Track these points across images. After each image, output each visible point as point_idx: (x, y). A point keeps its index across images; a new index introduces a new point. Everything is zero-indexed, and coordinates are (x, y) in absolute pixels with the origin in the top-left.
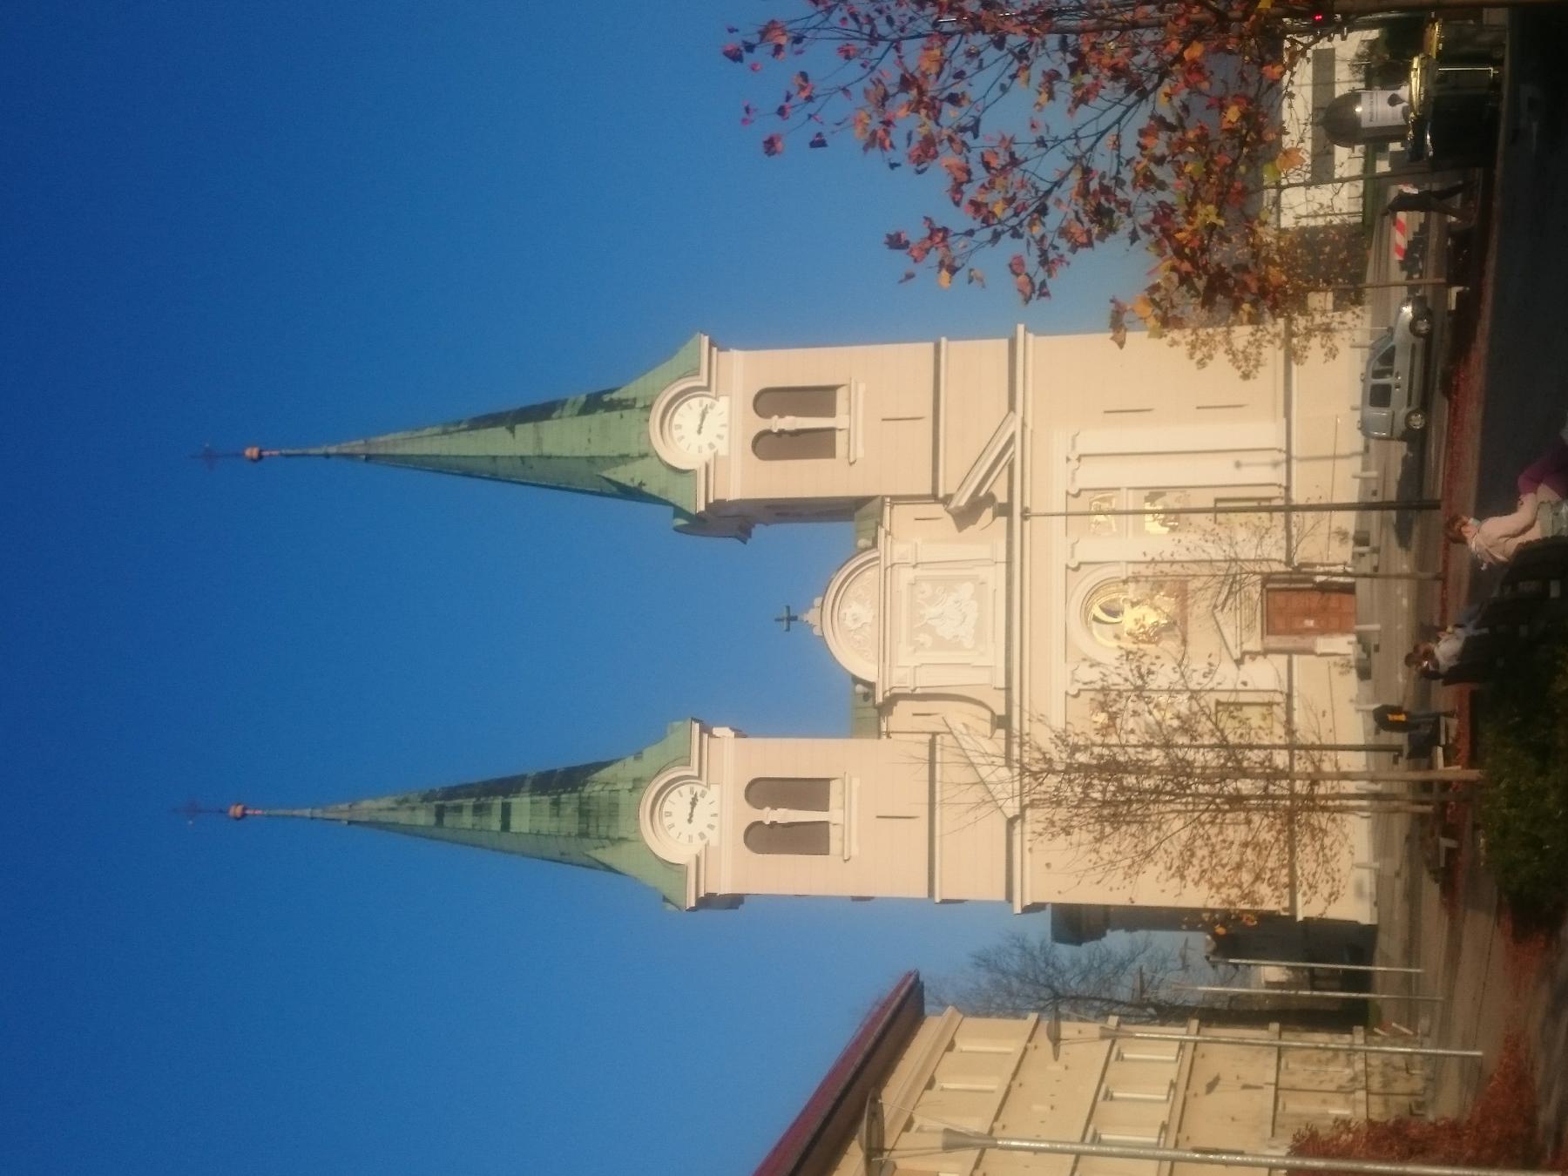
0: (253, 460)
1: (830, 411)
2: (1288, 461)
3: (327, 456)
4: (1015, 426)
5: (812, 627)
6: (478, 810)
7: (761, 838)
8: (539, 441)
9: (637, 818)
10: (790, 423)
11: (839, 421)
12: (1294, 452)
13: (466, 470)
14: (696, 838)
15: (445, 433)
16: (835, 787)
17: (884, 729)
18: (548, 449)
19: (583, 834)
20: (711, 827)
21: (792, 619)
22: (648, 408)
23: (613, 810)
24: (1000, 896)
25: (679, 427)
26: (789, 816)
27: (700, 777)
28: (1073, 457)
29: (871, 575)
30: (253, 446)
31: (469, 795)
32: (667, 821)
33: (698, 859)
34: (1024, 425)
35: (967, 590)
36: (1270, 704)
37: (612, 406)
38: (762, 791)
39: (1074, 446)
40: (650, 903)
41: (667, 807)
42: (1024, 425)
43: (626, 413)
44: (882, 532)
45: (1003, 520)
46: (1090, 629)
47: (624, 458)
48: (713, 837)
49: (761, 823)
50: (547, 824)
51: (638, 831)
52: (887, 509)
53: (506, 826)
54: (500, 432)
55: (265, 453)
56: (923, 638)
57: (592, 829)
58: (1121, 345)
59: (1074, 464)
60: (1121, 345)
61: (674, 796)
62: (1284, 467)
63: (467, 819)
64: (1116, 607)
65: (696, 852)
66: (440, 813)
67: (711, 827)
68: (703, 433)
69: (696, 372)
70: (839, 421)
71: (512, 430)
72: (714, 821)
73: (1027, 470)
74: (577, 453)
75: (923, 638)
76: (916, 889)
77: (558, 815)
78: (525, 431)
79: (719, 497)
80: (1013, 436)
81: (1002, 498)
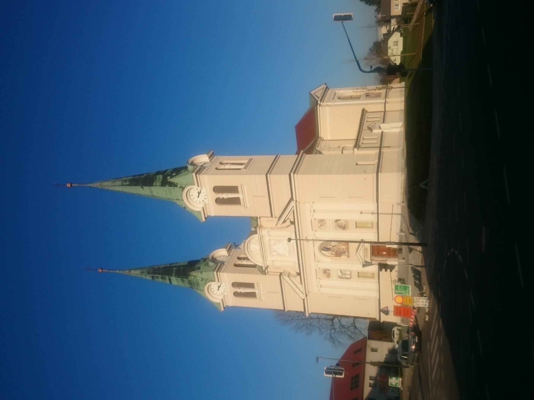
4: (293, 204)
6: (162, 278)
8: (152, 192)
12: (379, 212)
14: (202, 202)
15: (123, 185)
20: (205, 199)
22: (183, 189)
24: (303, 310)
25: (192, 195)
26: (244, 289)
33: (203, 208)
42: (296, 201)
48: (206, 201)
51: (182, 196)
52: (259, 220)
53: (171, 283)
56: (274, 253)
58: (320, 153)
59: (312, 212)
60: (320, 153)
62: (376, 215)
63: (160, 280)
64: (328, 247)
66: (153, 277)
67: (205, 199)
68: (199, 197)
72: (206, 197)
73: (297, 188)
75: (274, 253)
78: (146, 188)
79: (208, 215)
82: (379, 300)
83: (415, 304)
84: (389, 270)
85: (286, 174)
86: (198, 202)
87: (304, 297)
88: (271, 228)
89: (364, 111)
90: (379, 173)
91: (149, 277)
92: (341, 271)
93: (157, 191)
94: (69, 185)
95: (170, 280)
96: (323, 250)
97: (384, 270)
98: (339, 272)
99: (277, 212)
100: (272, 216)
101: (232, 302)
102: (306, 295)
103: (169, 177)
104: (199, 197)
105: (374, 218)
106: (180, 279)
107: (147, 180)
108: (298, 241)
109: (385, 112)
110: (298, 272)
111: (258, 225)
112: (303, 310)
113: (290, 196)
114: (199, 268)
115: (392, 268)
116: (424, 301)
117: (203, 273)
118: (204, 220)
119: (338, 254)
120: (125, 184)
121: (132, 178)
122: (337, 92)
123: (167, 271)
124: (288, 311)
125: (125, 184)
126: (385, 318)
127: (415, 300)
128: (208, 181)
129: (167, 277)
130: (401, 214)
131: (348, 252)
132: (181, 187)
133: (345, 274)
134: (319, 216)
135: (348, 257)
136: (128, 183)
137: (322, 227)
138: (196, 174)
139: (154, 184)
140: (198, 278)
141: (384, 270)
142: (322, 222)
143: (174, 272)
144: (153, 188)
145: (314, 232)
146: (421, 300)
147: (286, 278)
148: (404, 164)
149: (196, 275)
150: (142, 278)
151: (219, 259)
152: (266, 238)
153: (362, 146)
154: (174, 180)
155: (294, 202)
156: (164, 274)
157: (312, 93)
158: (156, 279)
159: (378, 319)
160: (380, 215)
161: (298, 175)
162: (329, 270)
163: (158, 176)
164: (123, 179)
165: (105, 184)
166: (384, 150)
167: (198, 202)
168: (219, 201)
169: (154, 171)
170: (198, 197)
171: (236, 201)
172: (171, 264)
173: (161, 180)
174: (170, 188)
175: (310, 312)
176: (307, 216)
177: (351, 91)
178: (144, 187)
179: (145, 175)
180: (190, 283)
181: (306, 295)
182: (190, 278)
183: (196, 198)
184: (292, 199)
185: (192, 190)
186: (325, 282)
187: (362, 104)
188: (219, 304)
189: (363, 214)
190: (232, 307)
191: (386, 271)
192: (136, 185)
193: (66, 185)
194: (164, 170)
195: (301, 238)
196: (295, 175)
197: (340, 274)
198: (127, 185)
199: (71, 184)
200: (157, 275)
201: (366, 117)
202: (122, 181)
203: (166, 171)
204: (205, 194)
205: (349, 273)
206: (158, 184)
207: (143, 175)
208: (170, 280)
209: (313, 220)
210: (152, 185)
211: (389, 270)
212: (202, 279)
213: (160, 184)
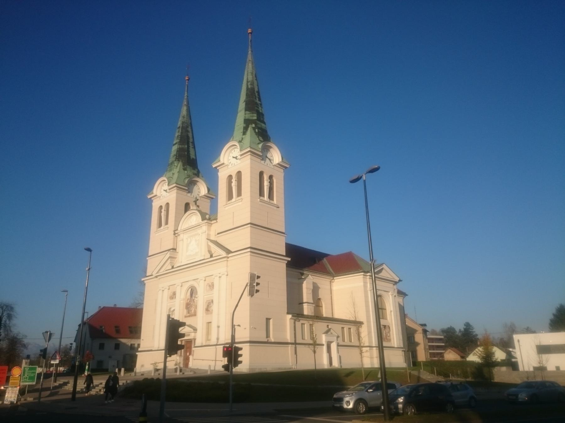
6: (178, 136)
8: (241, 111)
15: (248, 82)
24: (147, 275)
42: (228, 258)
63: (177, 134)
66: (179, 127)
75: (189, 240)
82: (151, 350)
83: (10, 389)
85: (251, 243)
87: (155, 275)
88: (209, 235)
89: (358, 324)
90: (248, 344)
91: (180, 124)
92: (174, 310)
93: (241, 115)
94: (250, 31)
95: (176, 144)
99: (221, 240)
101: (156, 205)
102: (156, 277)
103: (254, 125)
104: (233, 159)
109: (250, 342)
111: (211, 221)
112: (147, 275)
113: (233, 250)
114: (185, 169)
116: (12, 400)
118: (214, 166)
120: (249, 84)
121: (256, 89)
122: (390, 293)
123: (186, 140)
124: (147, 260)
125: (249, 84)
127: (15, 389)
130: (215, 370)
132: (242, 138)
136: (249, 87)
137: (208, 287)
139: (247, 112)
143: (183, 146)
144: (243, 111)
145: (204, 279)
146: (13, 396)
147: (168, 255)
148: (285, 369)
149: (178, 166)
150: (179, 117)
151: (195, 188)
152: (200, 231)
153: (298, 324)
155: (225, 255)
157: (384, 266)
158: (177, 130)
159: (139, 349)
160: (214, 347)
161: (249, 256)
163: (255, 115)
164: (255, 82)
165: (250, 65)
166: (290, 348)
169: (263, 110)
170: (233, 157)
172: (193, 143)
173: (251, 118)
176: (219, 268)
177: (392, 309)
179: (259, 102)
180: (172, 163)
181: (156, 277)
183: (232, 155)
184: (228, 252)
186: (167, 294)
187: (369, 321)
188: (153, 193)
194: (265, 121)
196: (249, 254)
197: (172, 310)
199: (251, 33)
201: (350, 326)
202: (253, 81)
203: (265, 123)
207: (260, 100)
208: (176, 144)
209: (213, 277)
213: (247, 118)
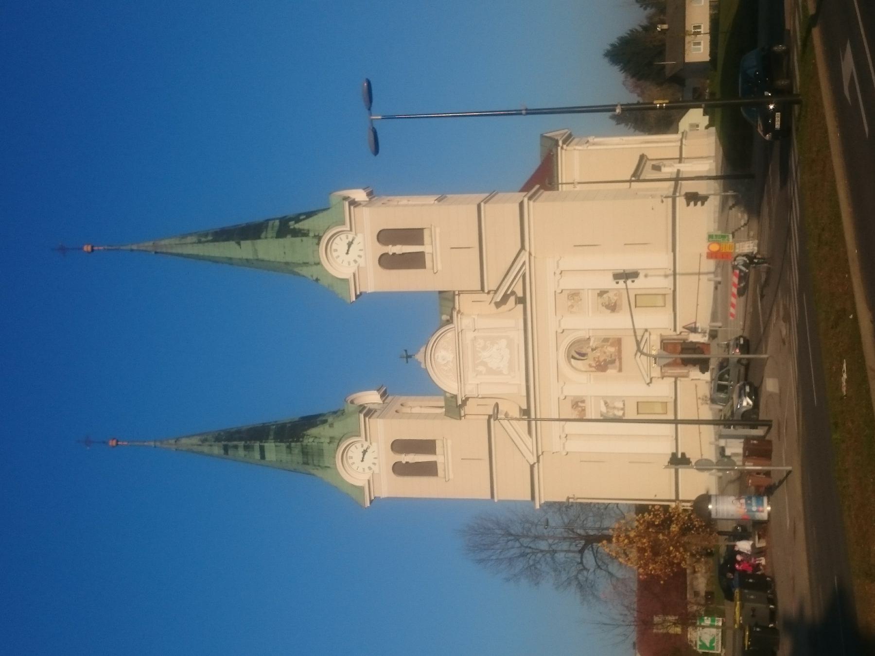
0: (88, 252)
1: (421, 242)
2: (675, 274)
3: (132, 250)
4: (524, 257)
5: (420, 363)
6: (246, 448)
7: (387, 262)
8: (255, 251)
9: (334, 457)
10: (399, 249)
11: (426, 248)
12: (677, 271)
13: (215, 260)
14: (367, 470)
15: (200, 242)
16: (426, 234)
17: (463, 414)
18: (261, 256)
19: (306, 463)
20: (360, 256)
21: (408, 357)
22: (319, 238)
23: (320, 453)
24: (528, 498)
26: (415, 456)
27: (351, 230)
28: (558, 272)
29: (450, 335)
30: (88, 244)
31: (241, 439)
32: (335, 254)
33: (369, 481)
34: (530, 254)
35: (503, 342)
36: (665, 295)
37: (296, 233)
38: (386, 236)
39: (558, 267)
40: (346, 500)
41: (334, 246)
42: (530, 254)
43: (304, 238)
44: (455, 314)
45: (521, 306)
46: (570, 362)
47: (306, 264)
49: (387, 254)
50: (285, 457)
52: (457, 297)
53: (263, 457)
54: (232, 244)
55: (95, 248)
56: (481, 368)
57: (310, 461)
59: (558, 276)
61: (337, 240)
62: (671, 278)
63: (241, 452)
64: (584, 351)
65: (353, 271)
66: (226, 449)
67: (374, 464)
68: (349, 256)
69: (344, 224)
70: (426, 248)
71: (239, 244)
72: (361, 253)
73: (535, 340)
74: (278, 260)
76: (484, 494)
77: (291, 453)
78: (247, 244)
79: (377, 495)
80: (524, 263)
81: (520, 294)
84: (699, 203)
86: (360, 470)
92: (606, 403)
93: (270, 249)
95: (262, 450)
96: (573, 357)
97: (692, 203)
98: (602, 403)
100: (483, 289)
101: (390, 487)
105: (668, 283)
106: (283, 445)
107: (252, 232)
108: (533, 423)
110: (525, 407)
113: (519, 246)
115: (703, 199)
117: (336, 425)
118: (368, 504)
119: (602, 367)
120: (203, 239)
123: (257, 435)
126: (695, 338)
128: (382, 432)
129: (257, 445)
131: (620, 359)
133: (614, 408)
134: (570, 283)
135: (620, 370)
136: (210, 238)
138: (365, 416)
139: (263, 235)
140: (322, 440)
141: (692, 203)
142: (574, 295)
143: (272, 433)
152: (469, 336)
154: (303, 225)
156: (250, 440)
160: (678, 277)
162: (583, 402)
167: (360, 470)
168: (400, 469)
171: (429, 470)
173: (276, 229)
174: (294, 239)
175: (543, 502)
178: (242, 242)
180: (305, 452)
181: (538, 457)
182: (305, 442)
185: (353, 448)
189: (649, 278)
190: (388, 498)
191: (695, 204)
192: (227, 240)
193: (82, 249)
195: (538, 417)
198: (208, 241)
200: (235, 443)
204: (361, 246)
205: (620, 405)
206: (269, 235)
210: (259, 238)
211: (699, 203)
212: (332, 439)
